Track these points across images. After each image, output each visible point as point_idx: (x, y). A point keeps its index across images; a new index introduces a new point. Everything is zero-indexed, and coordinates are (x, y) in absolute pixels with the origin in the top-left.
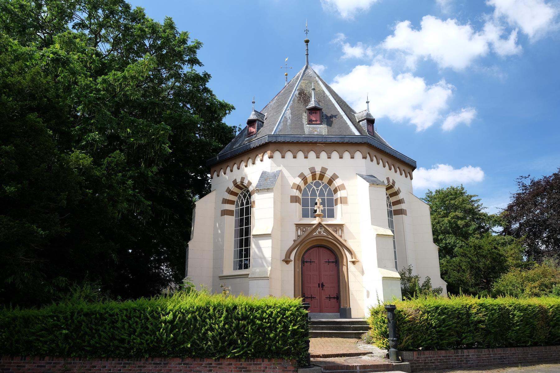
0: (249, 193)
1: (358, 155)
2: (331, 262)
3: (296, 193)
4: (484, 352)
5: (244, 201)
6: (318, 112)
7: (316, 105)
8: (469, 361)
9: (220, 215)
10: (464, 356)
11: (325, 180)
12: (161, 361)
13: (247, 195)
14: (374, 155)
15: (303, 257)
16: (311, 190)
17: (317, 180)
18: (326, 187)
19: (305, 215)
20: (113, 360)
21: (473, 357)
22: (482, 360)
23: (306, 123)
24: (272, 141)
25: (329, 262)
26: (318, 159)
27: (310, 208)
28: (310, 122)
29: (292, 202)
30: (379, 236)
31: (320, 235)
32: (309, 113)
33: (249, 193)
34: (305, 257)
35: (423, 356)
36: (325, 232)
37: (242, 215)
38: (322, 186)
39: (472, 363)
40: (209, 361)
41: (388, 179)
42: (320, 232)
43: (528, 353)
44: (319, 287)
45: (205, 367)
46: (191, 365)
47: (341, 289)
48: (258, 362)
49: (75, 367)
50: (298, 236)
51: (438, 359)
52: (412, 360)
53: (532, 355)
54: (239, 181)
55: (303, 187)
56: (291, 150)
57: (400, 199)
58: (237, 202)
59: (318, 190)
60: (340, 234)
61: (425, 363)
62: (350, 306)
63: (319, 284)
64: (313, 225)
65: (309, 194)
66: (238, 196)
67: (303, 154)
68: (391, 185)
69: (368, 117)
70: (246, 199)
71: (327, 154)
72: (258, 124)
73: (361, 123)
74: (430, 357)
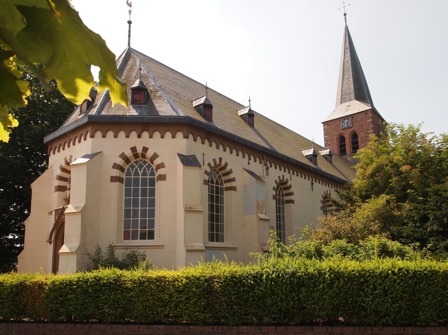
1: (180, 135)
3: (116, 173)
9: (54, 191)
24: (164, 123)
41: (221, 159)
53: (17, 331)
57: (231, 178)
65: (140, 174)
67: (171, 134)
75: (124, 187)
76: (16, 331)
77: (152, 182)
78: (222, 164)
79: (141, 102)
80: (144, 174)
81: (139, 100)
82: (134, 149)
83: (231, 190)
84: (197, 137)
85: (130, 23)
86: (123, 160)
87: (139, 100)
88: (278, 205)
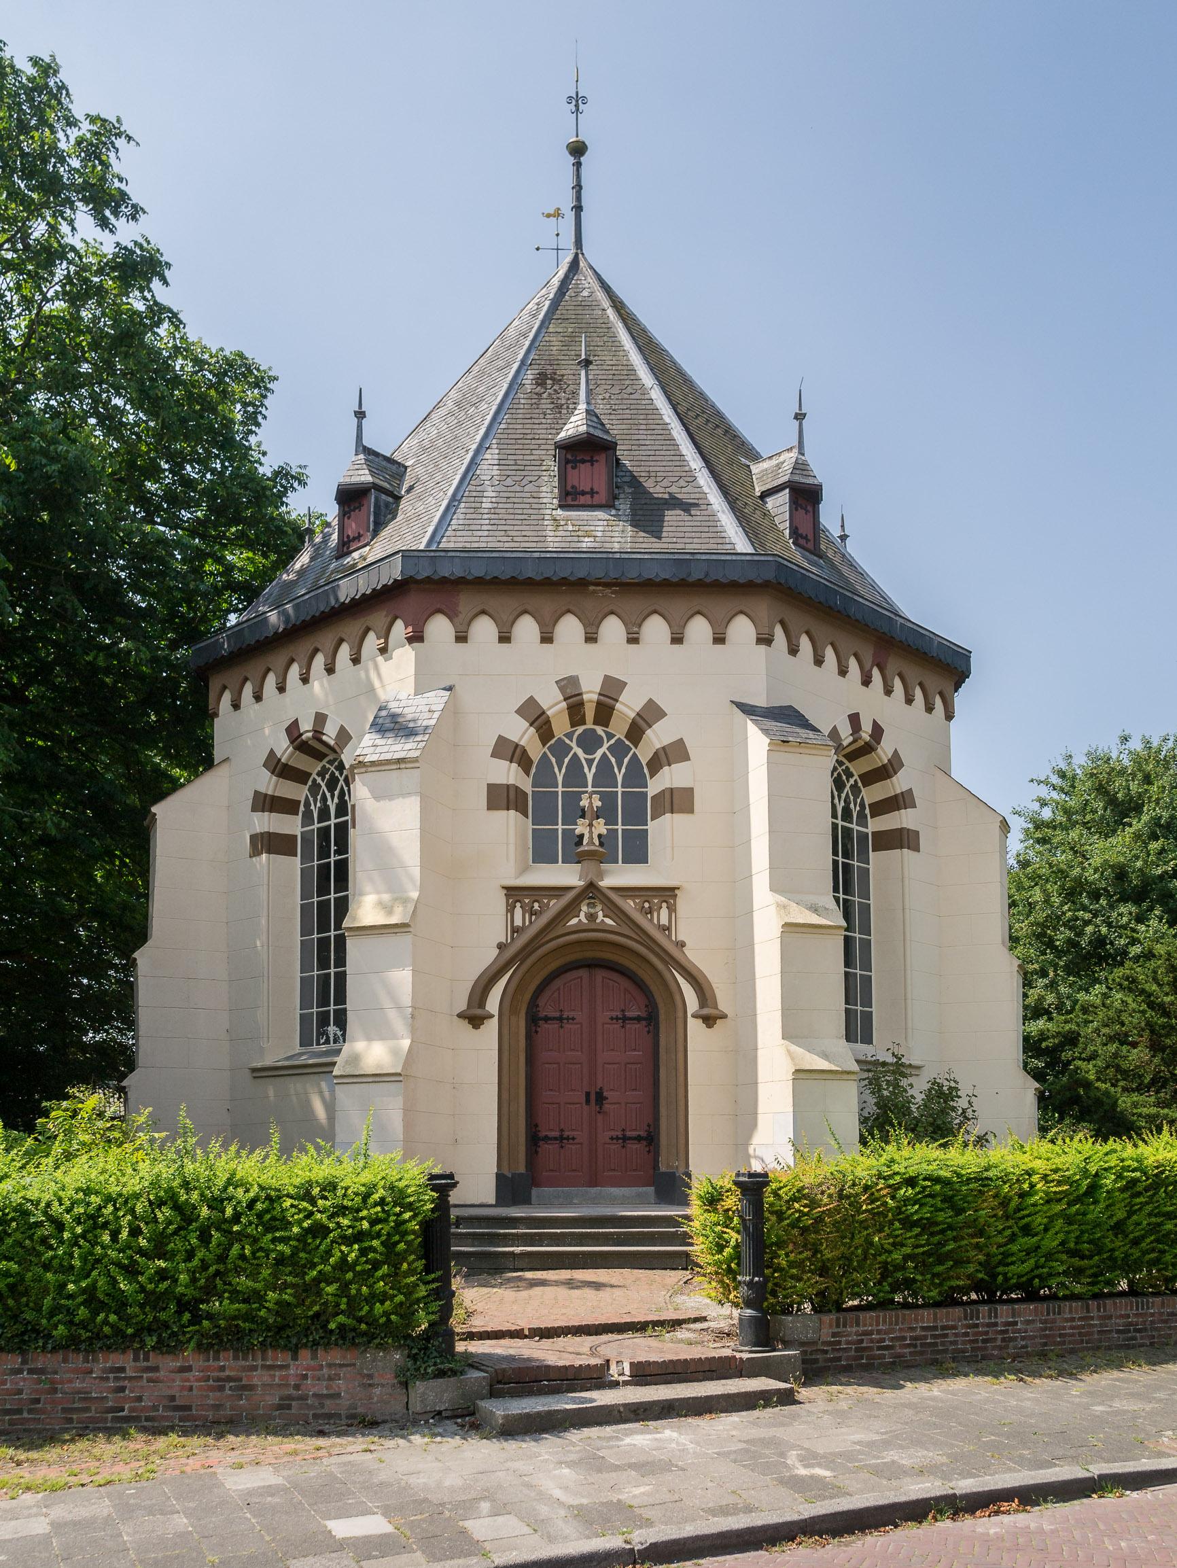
1: (742, 629)
2: (630, 1019)
3: (508, 773)
4: (1071, 1312)
5: (329, 802)
6: (602, 458)
7: (592, 431)
8: (1015, 1339)
10: (996, 1324)
11: (619, 728)
13: (341, 779)
14: (806, 628)
15: (533, 1004)
16: (567, 760)
17: (589, 725)
18: (619, 750)
19: (543, 852)
22: (1061, 1335)
23: (555, 501)
25: (625, 1019)
27: (560, 827)
28: (570, 497)
29: (492, 806)
30: (793, 929)
31: (593, 927)
32: (567, 462)
34: (541, 1002)
35: (854, 1329)
36: (611, 914)
37: (324, 853)
38: (606, 745)
39: (1023, 1347)
40: (116, 1359)
41: (854, 719)
42: (592, 917)
44: (588, 1101)
45: (102, 1378)
46: (56, 1373)
47: (663, 1111)
48: (277, 1359)
50: (515, 930)
51: (904, 1338)
52: (815, 1343)
54: (306, 726)
55: (536, 751)
56: (491, 611)
57: (898, 791)
58: (307, 804)
59: (590, 762)
61: (857, 1350)
63: (588, 1094)
64: (568, 889)
66: (310, 783)
68: (866, 743)
69: (797, 478)
70: (336, 793)
72: (377, 506)
73: (771, 502)
74: (879, 1332)
75: (531, 827)
77: (637, 810)
79: (597, 499)
80: (605, 774)
81: (588, 489)
83: (901, 847)
84: (798, 638)
85: (578, 150)
86: (531, 725)
87: (588, 489)
88: (840, 859)
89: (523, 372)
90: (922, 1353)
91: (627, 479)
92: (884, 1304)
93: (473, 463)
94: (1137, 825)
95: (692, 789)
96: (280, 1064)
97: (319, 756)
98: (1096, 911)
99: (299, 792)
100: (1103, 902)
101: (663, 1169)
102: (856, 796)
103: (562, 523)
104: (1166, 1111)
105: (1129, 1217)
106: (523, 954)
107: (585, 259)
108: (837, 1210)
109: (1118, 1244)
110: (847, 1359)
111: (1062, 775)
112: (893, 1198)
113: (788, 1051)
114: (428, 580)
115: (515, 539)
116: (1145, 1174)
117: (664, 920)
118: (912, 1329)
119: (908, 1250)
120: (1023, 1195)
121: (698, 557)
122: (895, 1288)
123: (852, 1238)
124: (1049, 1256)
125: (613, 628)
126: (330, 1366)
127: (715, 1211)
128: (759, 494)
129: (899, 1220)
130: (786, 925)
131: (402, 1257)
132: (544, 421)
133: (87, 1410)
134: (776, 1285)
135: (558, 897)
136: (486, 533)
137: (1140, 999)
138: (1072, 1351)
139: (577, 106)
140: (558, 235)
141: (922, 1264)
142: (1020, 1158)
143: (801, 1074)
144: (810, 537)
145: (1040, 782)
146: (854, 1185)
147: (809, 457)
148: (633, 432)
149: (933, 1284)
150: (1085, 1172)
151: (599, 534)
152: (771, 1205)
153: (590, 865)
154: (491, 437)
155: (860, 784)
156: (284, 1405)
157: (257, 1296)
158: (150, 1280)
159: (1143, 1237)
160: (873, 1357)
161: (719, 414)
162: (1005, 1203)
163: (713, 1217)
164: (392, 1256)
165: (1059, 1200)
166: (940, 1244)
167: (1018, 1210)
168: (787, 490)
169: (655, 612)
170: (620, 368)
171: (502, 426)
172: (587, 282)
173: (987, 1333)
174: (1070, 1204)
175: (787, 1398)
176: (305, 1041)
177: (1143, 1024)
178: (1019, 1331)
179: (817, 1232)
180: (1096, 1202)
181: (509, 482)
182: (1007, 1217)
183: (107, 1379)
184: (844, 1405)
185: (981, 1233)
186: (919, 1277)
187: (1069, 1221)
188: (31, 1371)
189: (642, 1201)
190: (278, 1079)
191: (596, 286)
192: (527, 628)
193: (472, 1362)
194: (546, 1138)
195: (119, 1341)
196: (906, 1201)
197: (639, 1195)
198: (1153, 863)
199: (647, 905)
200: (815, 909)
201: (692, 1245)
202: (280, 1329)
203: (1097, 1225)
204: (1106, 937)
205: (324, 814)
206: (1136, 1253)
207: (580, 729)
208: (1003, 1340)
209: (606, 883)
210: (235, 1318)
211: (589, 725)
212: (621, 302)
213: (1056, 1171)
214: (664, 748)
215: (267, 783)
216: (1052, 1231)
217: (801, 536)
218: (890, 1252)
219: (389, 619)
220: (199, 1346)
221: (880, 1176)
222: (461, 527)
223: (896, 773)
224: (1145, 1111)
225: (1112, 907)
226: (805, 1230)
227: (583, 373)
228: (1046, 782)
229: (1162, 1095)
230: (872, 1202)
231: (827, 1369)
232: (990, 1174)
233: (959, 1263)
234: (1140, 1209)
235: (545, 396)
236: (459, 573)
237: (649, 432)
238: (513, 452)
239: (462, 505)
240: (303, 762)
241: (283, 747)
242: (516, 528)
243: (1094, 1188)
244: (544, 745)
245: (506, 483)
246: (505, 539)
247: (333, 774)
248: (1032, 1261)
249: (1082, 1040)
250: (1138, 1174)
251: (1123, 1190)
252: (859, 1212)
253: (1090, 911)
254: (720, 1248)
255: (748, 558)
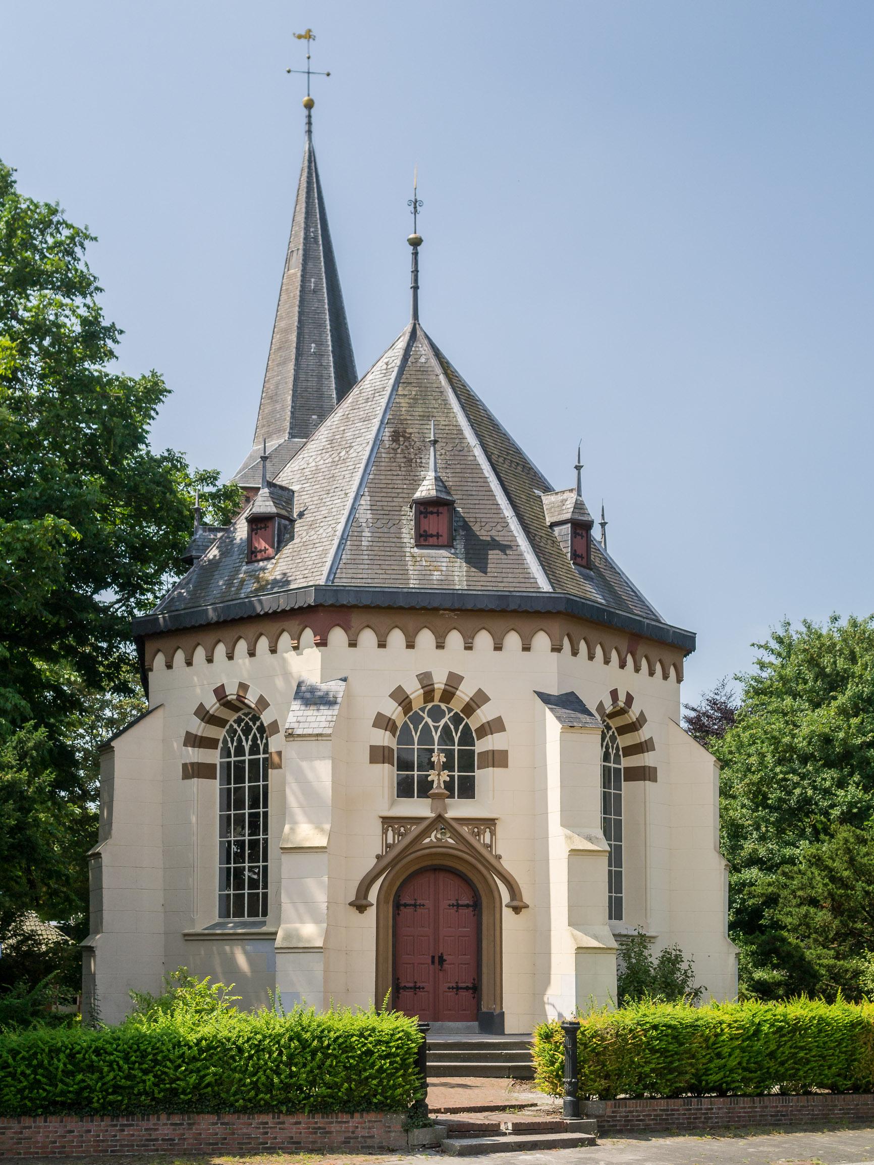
0: (258, 723)
1: (542, 641)
2: (462, 906)
3: (384, 738)
7: (440, 495)
8: (711, 1118)
12: (183, 1120)
13: (255, 728)
15: (398, 896)
19: (405, 789)
20: (102, 1121)
21: (720, 1111)
22: (738, 1117)
23: (412, 541)
25: (458, 906)
26: (440, 651)
28: (423, 539)
29: (373, 760)
32: (421, 513)
33: (258, 723)
38: (447, 717)
41: (614, 694)
43: (836, 1106)
44: (433, 962)
47: (485, 970)
49: (39, 1133)
50: (388, 846)
51: (651, 1115)
53: (843, 1109)
57: (643, 740)
58: (225, 741)
59: (436, 728)
60: (488, 841)
61: (625, 1121)
62: (502, 1008)
63: (433, 957)
66: (227, 727)
69: (576, 517)
70: (250, 737)
71: (464, 638)
72: (279, 524)
73: (557, 530)
74: (637, 1111)
75: (396, 772)
76: (840, 1110)
78: (630, 713)
80: (446, 735)
82: (425, 680)
83: (645, 780)
85: (416, 243)
89: (382, 429)
90: (660, 1124)
91: (461, 524)
92: (640, 1096)
93: (353, 508)
94: (842, 699)
95: (507, 751)
96: (206, 932)
97: (236, 709)
98: (804, 774)
99: (220, 734)
100: (810, 767)
101: (484, 1009)
102: (613, 743)
103: (418, 559)
104: (842, 962)
105: (778, 1049)
106: (393, 863)
107: (421, 329)
108: (615, 1043)
109: (772, 1064)
110: (620, 1126)
111: (780, 640)
112: (645, 1036)
113: (573, 935)
114: (332, 606)
115: (387, 572)
116: (788, 1023)
117: (488, 841)
118: (656, 1110)
119: (653, 1066)
120: (717, 1035)
121: (514, 594)
122: (646, 1087)
123: (623, 1059)
124: (731, 1071)
125: (455, 639)
126: (369, 1121)
127: (549, 1042)
128: (548, 524)
129: (649, 1049)
130: (572, 850)
131: (408, 1066)
132: (400, 473)
133: (250, 1143)
134: (583, 1084)
135: (417, 824)
136: (367, 567)
137: (823, 874)
138: (745, 1126)
139: (415, 208)
140: (309, 58)
141: (659, 1073)
142: (717, 1013)
143: (580, 950)
144: (585, 555)
145: (760, 647)
146: (624, 1029)
147: (585, 498)
148: (462, 484)
149: (666, 1085)
150: (753, 1023)
151: (444, 569)
152: (581, 1040)
153: (438, 802)
154: (364, 485)
155: (616, 734)
156: (346, 1142)
157: (338, 1086)
158: (286, 1078)
159: (787, 1061)
160: (634, 1125)
161: (518, 452)
162: (707, 1039)
163: (547, 1046)
164: (404, 1065)
165: (737, 1039)
166: (671, 1062)
167: (714, 1044)
168: (569, 525)
169: (484, 628)
170: (451, 427)
171: (371, 477)
172: (423, 349)
173: (696, 1114)
174: (743, 1041)
175: (592, 1143)
176: (225, 913)
177: (826, 894)
178: (714, 1113)
179: (604, 1055)
180: (758, 1040)
181: (379, 524)
182: (708, 1048)
183: (259, 1128)
184: (622, 1147)
185: (693, 1057)
186: (659, 1081)
187: (743, 1050)
188: (222, 1124)
189: (469, 1031)
190: (206, 942)
191: (431, 354)
192: (397, 638)
193: (436, 1122)
194: (405, 988)
195: (268, 1108)
196: (652, 1038)
197: (468, 1028)
198: (853, 734)
199: (476, 830)
200: (590, 839)
201: (532, 1061)
202: (346, 1102)
203: (759, 1052)
204: (812, 798)
205: (240, 751)
206: (782, 1070)
207: (430, 705)
208: (705, 1118)
209: (450, 814)
210: (325, 1097)
211: (436, 703)
212: (448, 363)
213: (736, 1021)
214: (488, 722)
215: (198, 727)
216: (733, 1057)
217: (579, 556)
218: (643, 1067)
219: (301, 627)
220: (310, 1112)
221: (638, 1024)
222: (349, 561)
223: (641, 727)
224: (825, 962)
225: (817, 771)
226: (598, 1054)
227: (432, 448)
228: (766, 647)
229: (842, 947)
230: (634, 1039)
231: (610, 1130)
232: (698, 1023)
233: (681, 1073)
234: (785, 1044)
235: (399, 451)
236: (353, 601)
237: (475, 484)
238: (379, 499)
239: (349, 543)
240: (225, 713)
241: (211, 704)
242: (387, 563)
243: (757, 1032)
244: (405, 716)
245: (376, 525)
246: (380, 572)
247: (247, 723)
248: (722, 1073)
249: (781, 901)
250: (783, 1024)
251: (774, 1033)
252: (627, 1044)
253: (799, 774)
254: (552, 1063)
255: (548, 595)
